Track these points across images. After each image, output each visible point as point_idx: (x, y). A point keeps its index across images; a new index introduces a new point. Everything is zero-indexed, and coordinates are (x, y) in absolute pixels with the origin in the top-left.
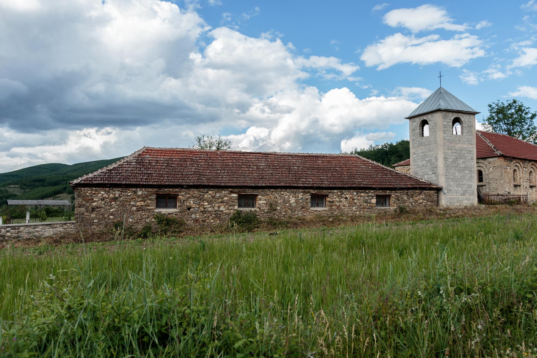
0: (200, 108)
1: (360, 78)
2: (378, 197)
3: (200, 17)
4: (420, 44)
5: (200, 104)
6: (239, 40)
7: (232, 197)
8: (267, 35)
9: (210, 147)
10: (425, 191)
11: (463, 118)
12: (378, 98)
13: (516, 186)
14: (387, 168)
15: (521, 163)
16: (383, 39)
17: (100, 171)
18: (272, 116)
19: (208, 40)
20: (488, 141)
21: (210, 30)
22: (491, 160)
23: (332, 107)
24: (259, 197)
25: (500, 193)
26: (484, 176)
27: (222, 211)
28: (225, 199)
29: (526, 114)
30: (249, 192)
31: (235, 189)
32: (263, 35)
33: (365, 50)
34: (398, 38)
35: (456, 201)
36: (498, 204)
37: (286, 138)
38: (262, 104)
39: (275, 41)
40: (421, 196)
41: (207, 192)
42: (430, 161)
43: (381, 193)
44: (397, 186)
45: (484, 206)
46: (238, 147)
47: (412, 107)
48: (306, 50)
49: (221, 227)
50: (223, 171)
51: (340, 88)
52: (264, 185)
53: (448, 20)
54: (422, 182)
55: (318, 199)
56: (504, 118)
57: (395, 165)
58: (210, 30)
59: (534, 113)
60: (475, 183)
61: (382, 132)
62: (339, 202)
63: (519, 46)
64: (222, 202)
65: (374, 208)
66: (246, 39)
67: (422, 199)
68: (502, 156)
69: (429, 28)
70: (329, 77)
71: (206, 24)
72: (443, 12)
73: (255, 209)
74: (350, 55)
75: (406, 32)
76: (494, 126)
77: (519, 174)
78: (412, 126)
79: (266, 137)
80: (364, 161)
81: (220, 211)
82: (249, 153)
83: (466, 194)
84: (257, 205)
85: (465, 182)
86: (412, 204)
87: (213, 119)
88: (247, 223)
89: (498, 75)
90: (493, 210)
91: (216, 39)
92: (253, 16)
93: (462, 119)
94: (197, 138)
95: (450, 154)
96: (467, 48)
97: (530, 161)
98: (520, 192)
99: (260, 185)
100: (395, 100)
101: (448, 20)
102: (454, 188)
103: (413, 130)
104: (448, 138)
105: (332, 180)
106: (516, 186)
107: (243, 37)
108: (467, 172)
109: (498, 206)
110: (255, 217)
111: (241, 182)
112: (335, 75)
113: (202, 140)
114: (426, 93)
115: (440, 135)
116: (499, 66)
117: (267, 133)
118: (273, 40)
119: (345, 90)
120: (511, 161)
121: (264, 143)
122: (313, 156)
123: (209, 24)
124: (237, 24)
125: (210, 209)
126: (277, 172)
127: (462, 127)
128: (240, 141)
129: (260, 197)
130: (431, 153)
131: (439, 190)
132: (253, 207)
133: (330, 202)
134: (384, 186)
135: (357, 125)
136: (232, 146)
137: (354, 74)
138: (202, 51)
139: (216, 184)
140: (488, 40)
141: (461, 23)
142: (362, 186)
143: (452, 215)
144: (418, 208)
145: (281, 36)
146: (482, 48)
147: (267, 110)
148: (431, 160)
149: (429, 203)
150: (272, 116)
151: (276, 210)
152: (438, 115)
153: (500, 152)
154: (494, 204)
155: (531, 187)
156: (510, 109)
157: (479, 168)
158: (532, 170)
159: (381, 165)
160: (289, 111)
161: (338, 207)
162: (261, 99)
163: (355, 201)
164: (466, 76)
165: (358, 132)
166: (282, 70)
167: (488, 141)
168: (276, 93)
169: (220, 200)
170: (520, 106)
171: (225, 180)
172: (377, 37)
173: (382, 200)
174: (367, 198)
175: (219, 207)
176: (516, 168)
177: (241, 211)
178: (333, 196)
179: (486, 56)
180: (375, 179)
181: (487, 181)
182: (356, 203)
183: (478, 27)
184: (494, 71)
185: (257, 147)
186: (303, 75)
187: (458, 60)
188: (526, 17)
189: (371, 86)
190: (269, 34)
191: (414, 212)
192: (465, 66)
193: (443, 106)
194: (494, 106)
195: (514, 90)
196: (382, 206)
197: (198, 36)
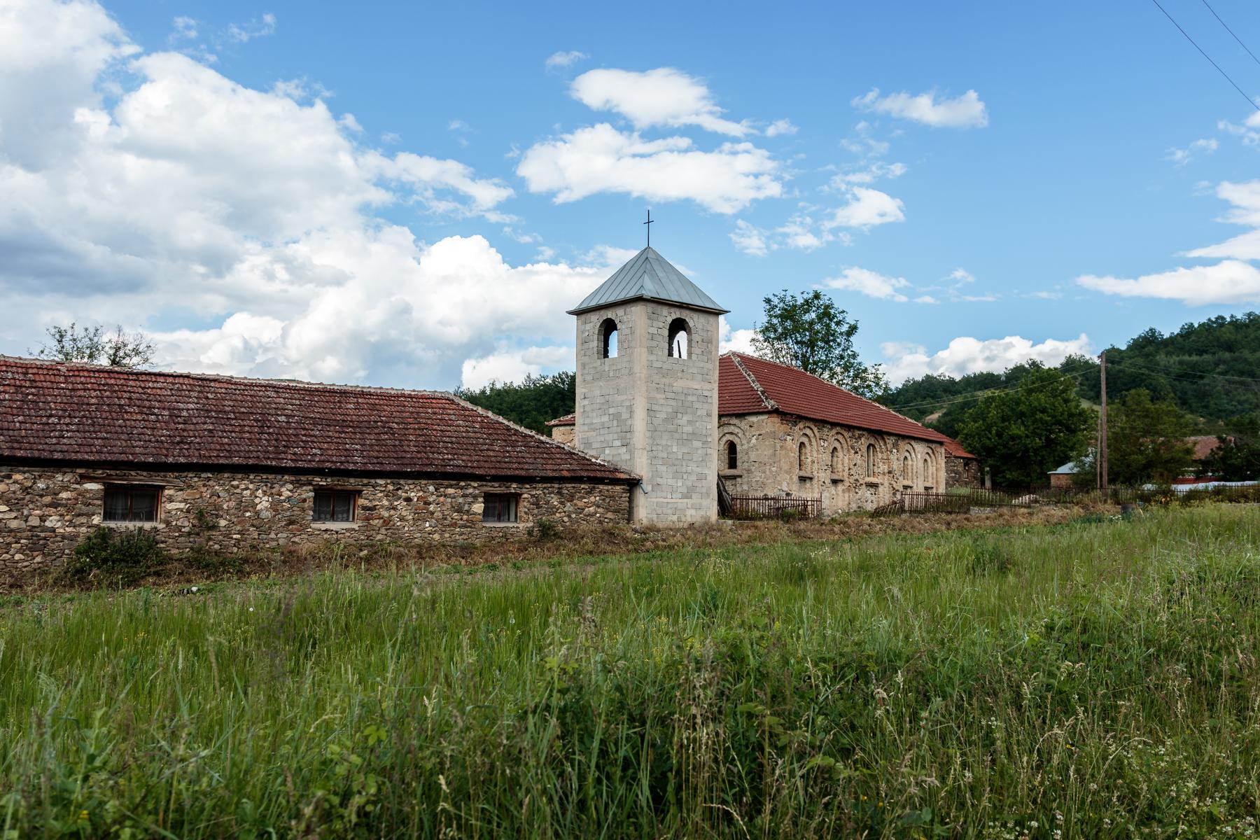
0: (97, 255)
1: (515, 218)
2: (488, 498)
3: (112, 18)
4: (650, 155)
5: (96, 243)
6: (216, 91)
7: (87, 491)
8: (291, 87)
9: (91, 356)
10: (601, 487)
11: (693, 320)
12: (554, 267)
13: (803, 479)
14: (517, 427)
15: (816, 430)
16: (571, 133)
17: (533, 433)
18: (294, 290)
19: (133, 82)
20: (751, 378)
21: (137, 56)
22: (753, 419)
23: (446, 280)
24: (166, 492)
25: (771, 495)
26: (739, 456)
27: (53, 530)
28: (64, 495)
29: (838, 323)
30: (139, 479)
31: (95, 470)
32: (280, 85)
33: (530, 153)
34: (604, 133)
35: (669, 511)
36: (761, 519)
37: (329, 348)
38: (268, 259)
39: (311, 104)
40: (592, 499)
41: (9, 477)
42: (617, 416)
43: (495, 488)
44: (536, 473)
45: (730, 522)
46: (199, 363)
47: (583, 284)
48: (389, 137)
49: (46, 573)
50: (67, 420)
51: (465, 235)
52: (182, 460)
53: (710, 108)
54: (595, 464)
55: (333, 501)
56: (796, 329)
57: (553, 422)
58: (137, 56)
59: (853, 323)
60: (714, 466)
61: (560, 346)
62: (388, 509)
63: (849, 183)
64: (54, 505)
65: (480, 525)
66: (234, 90)
67: (594, 504)
68: (775, 412)
69: (671, 121)
70: (442, 206)
71: (126, 39)
72: (702, 91)
73: (154, 524)
74: (493, 162)
75: (622, 123)
76: (777, 345)
77: (812, 453)
78: (583, 332)
79: (274, 342)
80: (464, 409)
81: (45, 529)
82: (155, 374)
83: (694, 496)
84: (161, 515)
85: (692, 467)
86: (569, 516)
87: (131, 285)
88: (125, 562)
89: (806, 240)
90: (749, 532)
91: (152, 81)
92: (257, 34)
93: (691, 324)
94: (53, 331)
95: (662, 402)
96: (747, 175)
97: (834, 425)
98: (808, 494)
99: (170, 460)
100: (591, 275)
101: (710, 108)
102: (667, 480)
103: (583, 342)
104: (659, 365)
105: (375, 454)
106: (803, 479)
107: (227, 84)
108: (697, 444)
109: (759, 523)
110: (151, 547)
111: (115, 450)
112: (456, 204)
113: (68, 337)
114: (621, 256)
115: (641, 356)
116: (809, 220)
117: (280, 332)
118: (306, 102)
119: (478, 242)
120: (795, 424)
121: (270, 355)
122: (332, 392)
123: (134, 40)
124: (212, 51)
125: (14, 524)
126: (227, 428)
127: (690, 341)
128: (205, 348)
129: (172, 492)
130: (620, 398)
131: (633, 484)
132: (150, 517)
133: (365, 508)
134: (503, 473)
135: (504, 327)
136: (154, 359)
137: (501, 207)
138: (110, 104)
139: (36, 454)
140: (789, 162)
141: (738, 121)
142: (449, 469)
143: (661, 543)
144: (584, 526)
145: (328, 94)
146: (777, 178)
147: (280, 272)
148: (619, 414)
149: (610, 515)
150: (294, 290)
151: (214, 527)
152: (638, 311)
153: (772, 402)
154: (752, 519)
155: (835, 482)
156: (807, 311)
157: (729, 437)
158: (837, 445)
159: (506, 422)
160: (339, 280)
161: (387, 522)
162: (267, 245)
163: (432, 508)
164: (743, 236)
165: (504, 342)
166: (326, 179)
167: (751, 378)
168: (308, 234)
169: (48, 499)
170: (827, 307)
171: (68, 442)
172: (557, 126)
173: (500, 505)
174: (461, 500)
175: (43, 519)
176: (805, 440)
177: (110, 529)
178: (376, 495)
179: (785, 196)
180: (485, 453)
181: (746, 466)
182: (432, 513)
183: (771, 131)
184: (799, 230)
185: (249, 366)
186: (379, 197)
187: (728, 200)
188: (862, 125)
189: (540, 239)
190: (297, 87)
191: (574, 536)
192: (742, 214)
193: (650, 290)
194: (775, 301)
195: (837, 274)
196: (499, 520)
197: (103, 66)
